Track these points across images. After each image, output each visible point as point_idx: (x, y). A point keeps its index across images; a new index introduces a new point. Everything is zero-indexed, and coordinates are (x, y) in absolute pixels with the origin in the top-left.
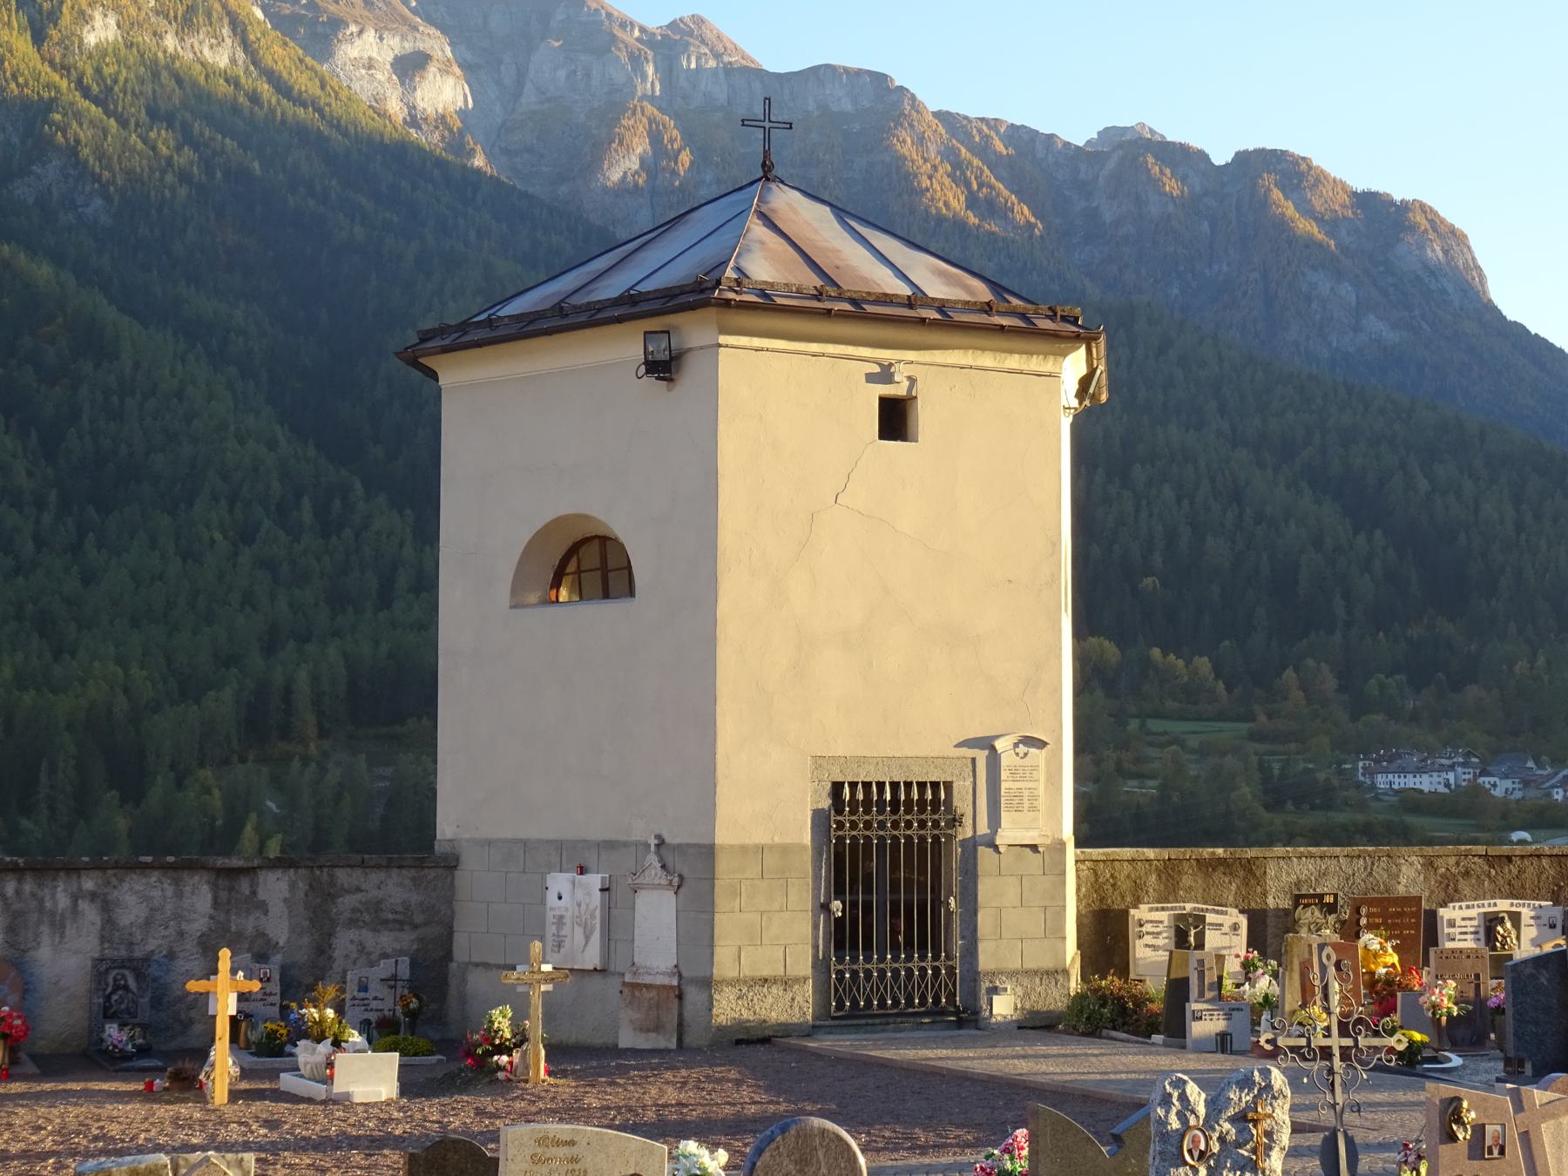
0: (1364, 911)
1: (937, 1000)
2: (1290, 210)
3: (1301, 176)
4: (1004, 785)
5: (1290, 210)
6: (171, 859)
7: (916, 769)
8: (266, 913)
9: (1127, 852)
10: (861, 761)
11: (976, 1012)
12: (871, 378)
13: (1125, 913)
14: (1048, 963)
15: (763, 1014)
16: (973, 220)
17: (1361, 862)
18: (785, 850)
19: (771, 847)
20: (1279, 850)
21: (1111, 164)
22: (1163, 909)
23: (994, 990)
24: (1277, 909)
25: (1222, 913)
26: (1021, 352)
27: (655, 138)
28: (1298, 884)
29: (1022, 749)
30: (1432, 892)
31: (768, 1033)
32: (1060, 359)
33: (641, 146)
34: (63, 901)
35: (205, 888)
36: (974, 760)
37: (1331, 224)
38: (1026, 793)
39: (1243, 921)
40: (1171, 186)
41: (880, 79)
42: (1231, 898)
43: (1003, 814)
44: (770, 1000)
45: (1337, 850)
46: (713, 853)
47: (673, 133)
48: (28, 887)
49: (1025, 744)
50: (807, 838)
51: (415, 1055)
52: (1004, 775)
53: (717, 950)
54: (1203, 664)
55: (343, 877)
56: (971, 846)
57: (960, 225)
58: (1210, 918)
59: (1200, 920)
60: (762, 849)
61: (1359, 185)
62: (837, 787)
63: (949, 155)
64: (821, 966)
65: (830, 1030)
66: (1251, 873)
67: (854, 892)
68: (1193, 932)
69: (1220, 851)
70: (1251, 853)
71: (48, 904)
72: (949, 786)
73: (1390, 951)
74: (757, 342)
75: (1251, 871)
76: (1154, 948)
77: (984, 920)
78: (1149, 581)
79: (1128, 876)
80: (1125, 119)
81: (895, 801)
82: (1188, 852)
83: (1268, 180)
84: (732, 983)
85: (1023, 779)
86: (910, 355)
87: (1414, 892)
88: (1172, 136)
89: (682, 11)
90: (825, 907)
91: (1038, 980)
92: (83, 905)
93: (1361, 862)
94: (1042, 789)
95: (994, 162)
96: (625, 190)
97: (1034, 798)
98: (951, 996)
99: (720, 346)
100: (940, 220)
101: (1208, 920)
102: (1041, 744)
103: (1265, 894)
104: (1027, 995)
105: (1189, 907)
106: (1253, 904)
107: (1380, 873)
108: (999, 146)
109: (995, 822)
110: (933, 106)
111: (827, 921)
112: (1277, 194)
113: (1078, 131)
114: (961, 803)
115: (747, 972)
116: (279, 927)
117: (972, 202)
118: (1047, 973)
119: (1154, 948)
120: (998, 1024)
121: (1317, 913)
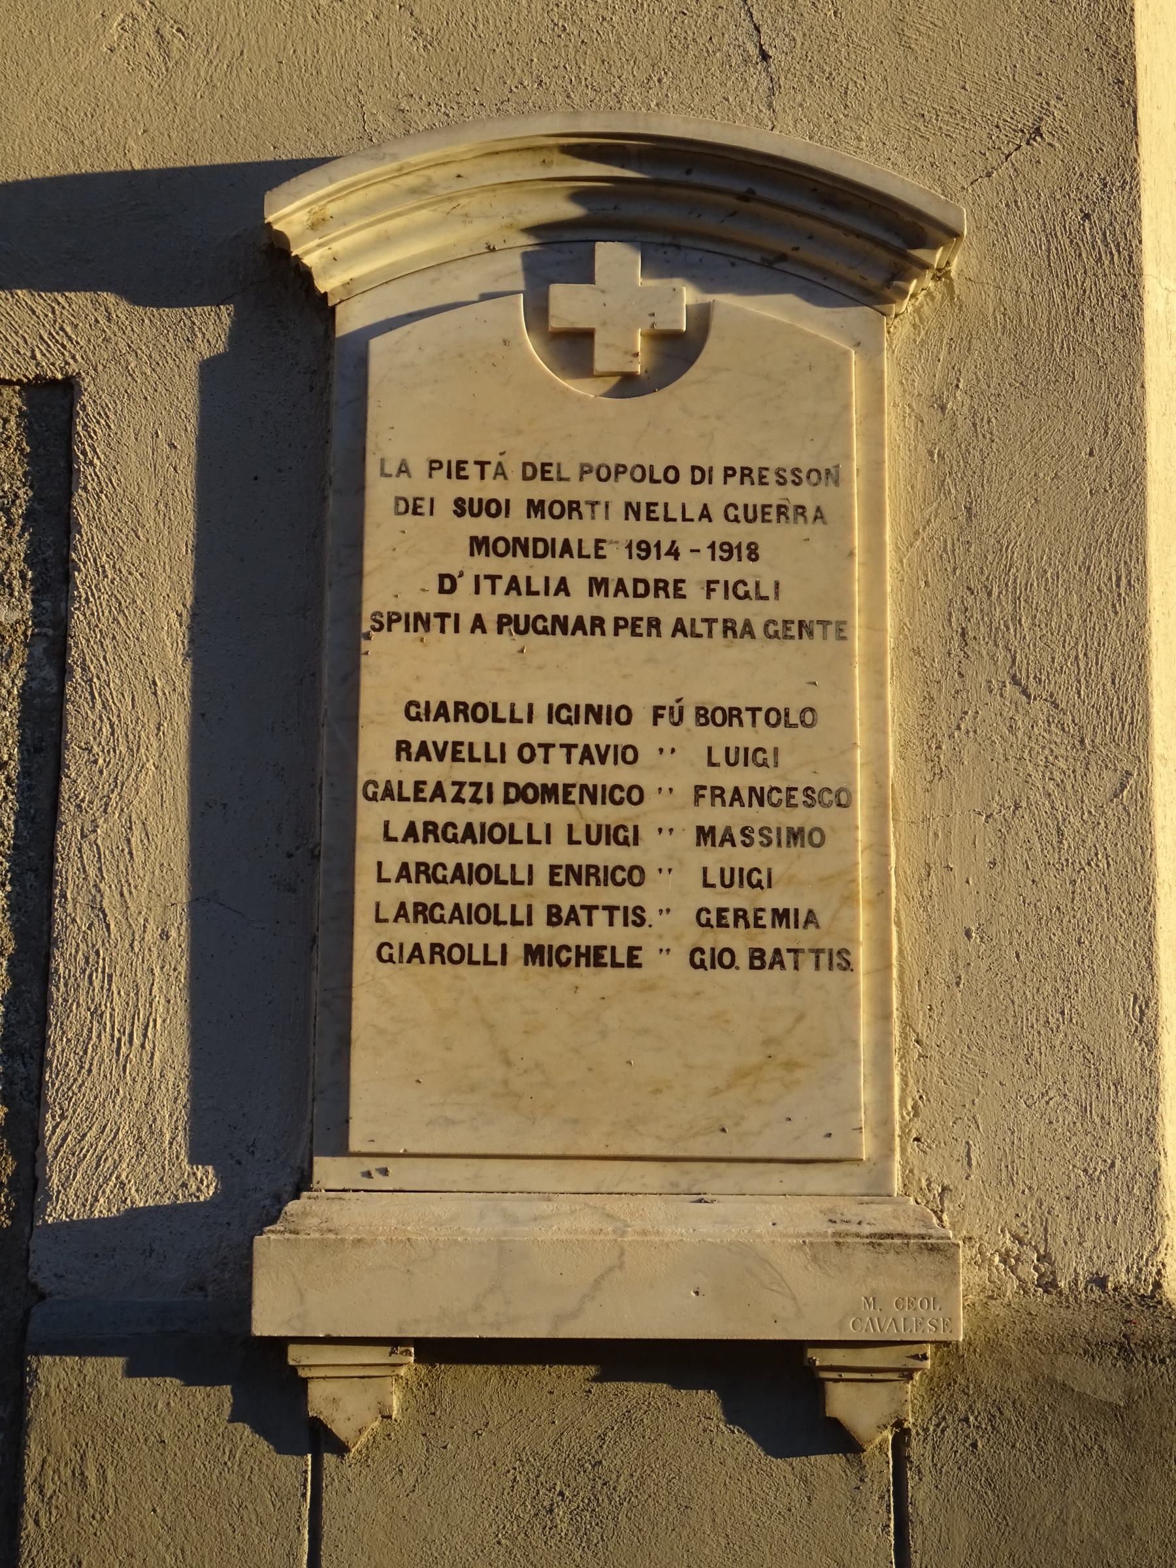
4: (392, 675)
29: (625, 294)
36: (52, 408)
38: (672, 766)
43: (380, 997)
49: (666, 251)
85: (640, 608)
97: (773, 805)
102: (847, 239)
109: (274, 1083)
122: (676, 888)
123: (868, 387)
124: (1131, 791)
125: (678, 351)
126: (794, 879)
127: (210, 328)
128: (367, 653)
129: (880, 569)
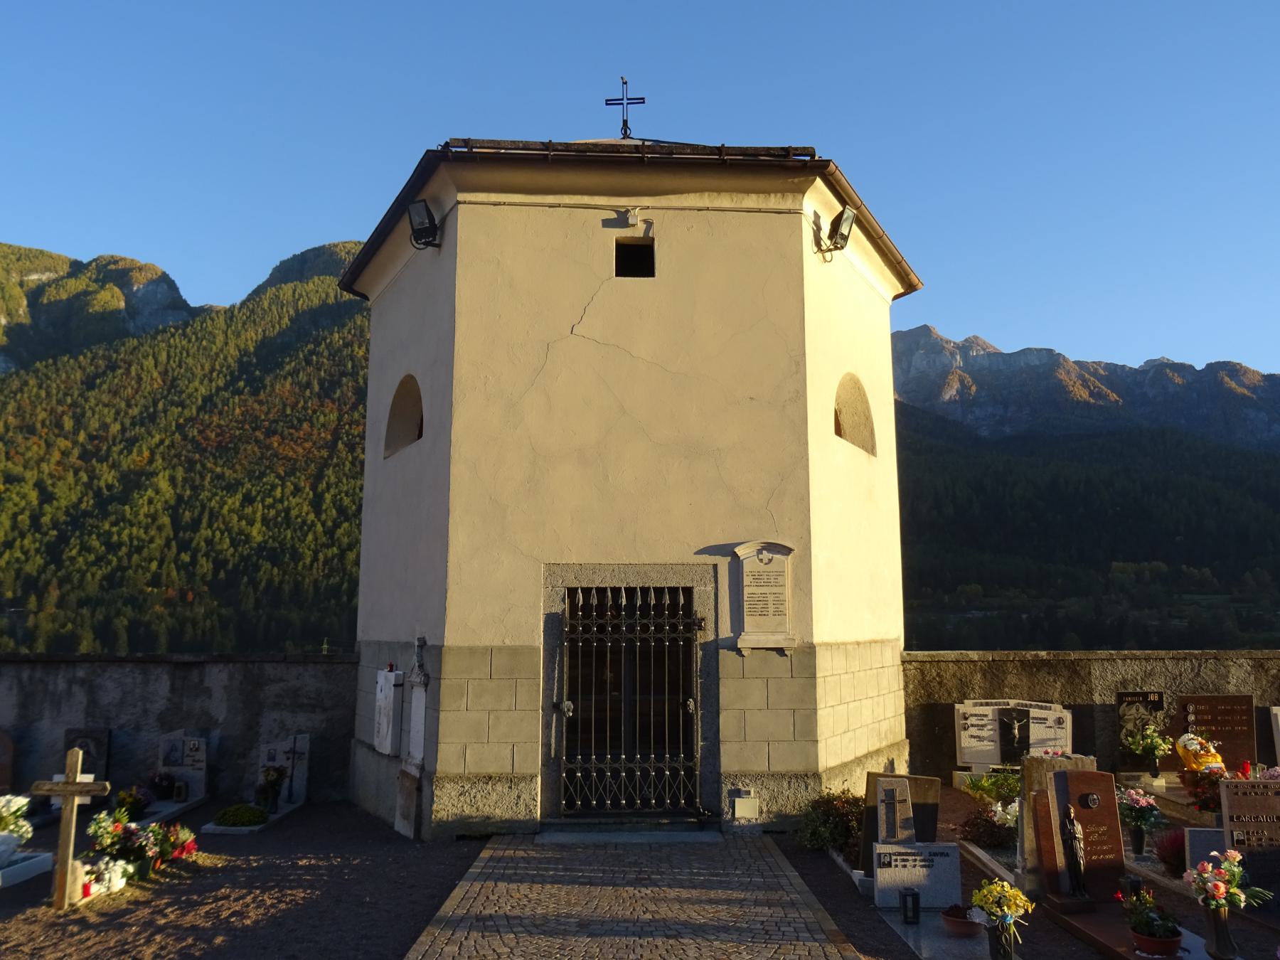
0: (1191, 708)
1: (675, 801)
2: (1233, 385)
3: (1237, 371)
4: (747, 591)
5: (1233, 385)
6: (139, 655)
7: (654, 575)
8: (210, 697)
9: (951, 655)
10: (596, 568)
11: (718, 813)
12: (607, 223)
13: (950, 709)
14: (797, 766)
15: (487, 811)
16: (1092, 401)
17: (1188, 664)
18: (514, 652)
19: (500, 649)
20: (1103, 653)
21: (1151, 374)
22: (987, 704)
23: (737, 793)
24: (1104, 705)
25: (1046, 708)
26: (758, 192)
27: (962, 382)
28: (1124, 683)
29: (766, 555)
30: (1264, 691)
31: (490, 829)
32: (799, 196)
33: (956, 385)
34: (61, 684)
35: (165, 677)
36: (715, 566)
37: (1253, 389)
38: (771, 598)
39: (1068, 716)
40: (1178, 380)
41: (1050, 351)
42: (1057, 695)
43: (747, 619)
44: (494, 796)
45: (1162, 653)
46: (440, 653)
47: (969, 380)
48: (38, 674)
49: (769, 551)
50: (539, 641)
51: (234, 825)
52: (747, 580)
53: (442, 747)
54: (1207, 571)
55: (270, 670)
56: (713, 649)
57: (1087, 403)
58: (1034, 713)
59: (1023, 715)
60: (491, 650)
61: (1266, 372)
62: (572, 592)
63: (1081, 377)
64: (550, 763)
65: (562, 828)
66: (1076, 674)
67: (587, 692)
68: (1017, 725)
69: (1043, 654)
70: (1073, 655)
71: (51, 687)
72: (688, 591)
73: (1213, 751)
74: (494, 197)
75: (1075, 672)
76: (980, 738)
77: (727, 722)
78: (1178, 538)
79: (954, 675)
80: (1155, 356)
81: (659, 605)
82: (1012, 655)
83: (1222, 374)
84: (454, 779)
85: (768, 584)
86: (646, 201)
87: (1245, 691)
88: (1177, 360)
89: (970, 334)
90: (557, 707)
91: (785, 784)
92: (76, 689)
93: (1188, 664)
94: (788, 592)
95: (1100, 378)
96: (951, 401)
97: (780, 602)
98: (690, 799)
99: (459, 203)
100: (1078, 402)
101: (1032, 715)
102: (787, 551)
103: (1091, 692)
104: (774, 798)
105: (1013, 703)
106: (1079, 701)
107: (1208, 673)
108: (1102, 372)
109: (738, 625)
110: (1072, 359)
111: (559, 721)
112: (1227, 379)
113: (1135, 362)
114: (702, 607)
115: (472, 768)
116: (219, 707)
117: (1091, 394)
118: (796, 776)
119: (980, 738)
120: (742, 827)
121: (1142, 710)
122: (771, 610)
123: (788, 562)
124: (810, 599)
125: (770, 560)
126: (781, 608)
127: (729, 559)
128: (635, 259)
129: (789, 580)
